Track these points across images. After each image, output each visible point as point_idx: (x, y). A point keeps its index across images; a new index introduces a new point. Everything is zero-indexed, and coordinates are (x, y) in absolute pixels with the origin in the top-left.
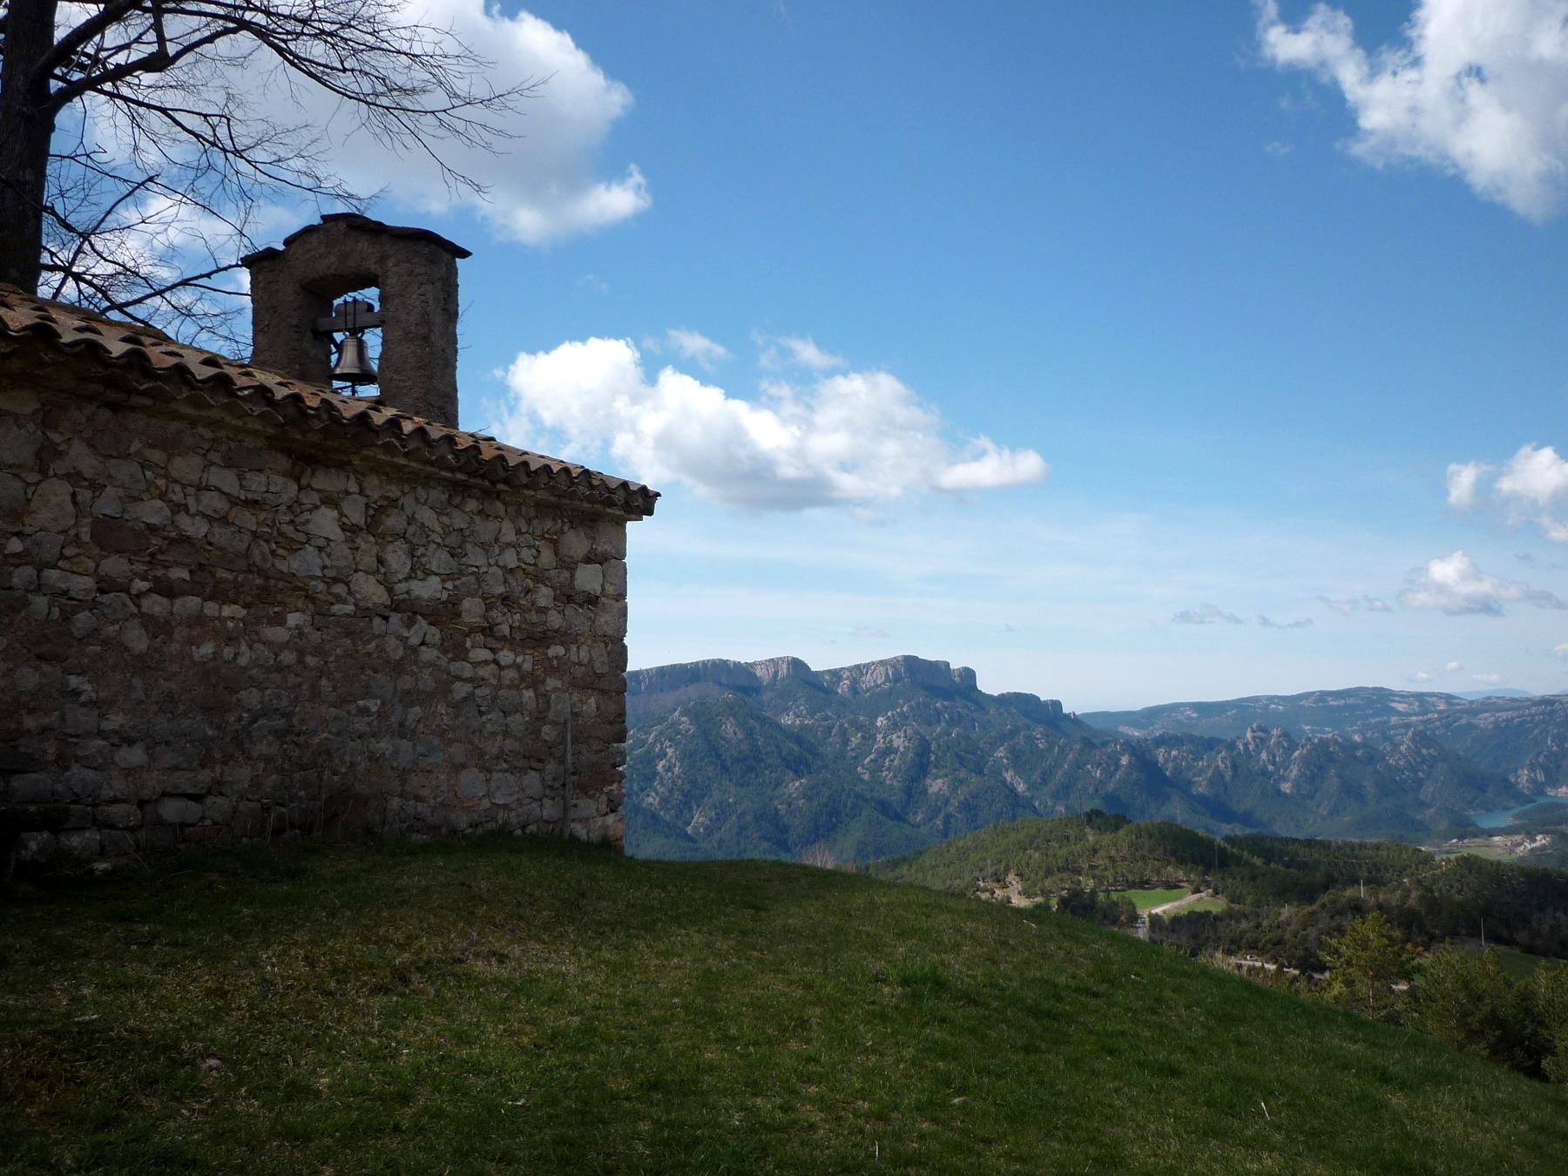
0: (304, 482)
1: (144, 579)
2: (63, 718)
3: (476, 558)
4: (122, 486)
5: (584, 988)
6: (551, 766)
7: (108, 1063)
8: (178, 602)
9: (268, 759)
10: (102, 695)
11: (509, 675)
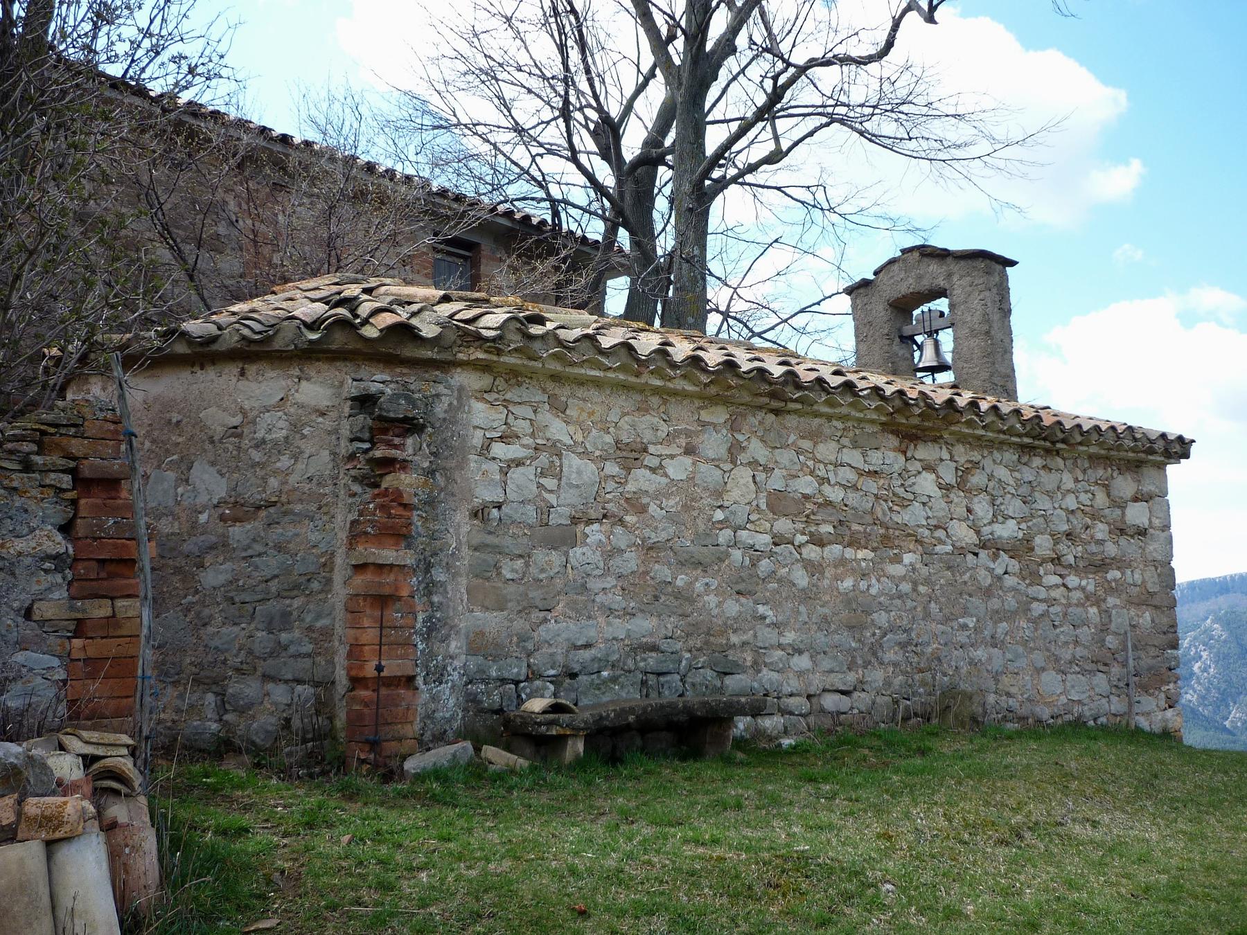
0: (909, 454)
1: (803, 534)
2: (755, 636)
3: (1043, 503)
4: (785, 468)
5: (1167, 852)
6: (1116, 670)
7: (819, 881)
8: (827, 549)
9: (895, 665)
10: (780, 618)
11: (1077, 595)
